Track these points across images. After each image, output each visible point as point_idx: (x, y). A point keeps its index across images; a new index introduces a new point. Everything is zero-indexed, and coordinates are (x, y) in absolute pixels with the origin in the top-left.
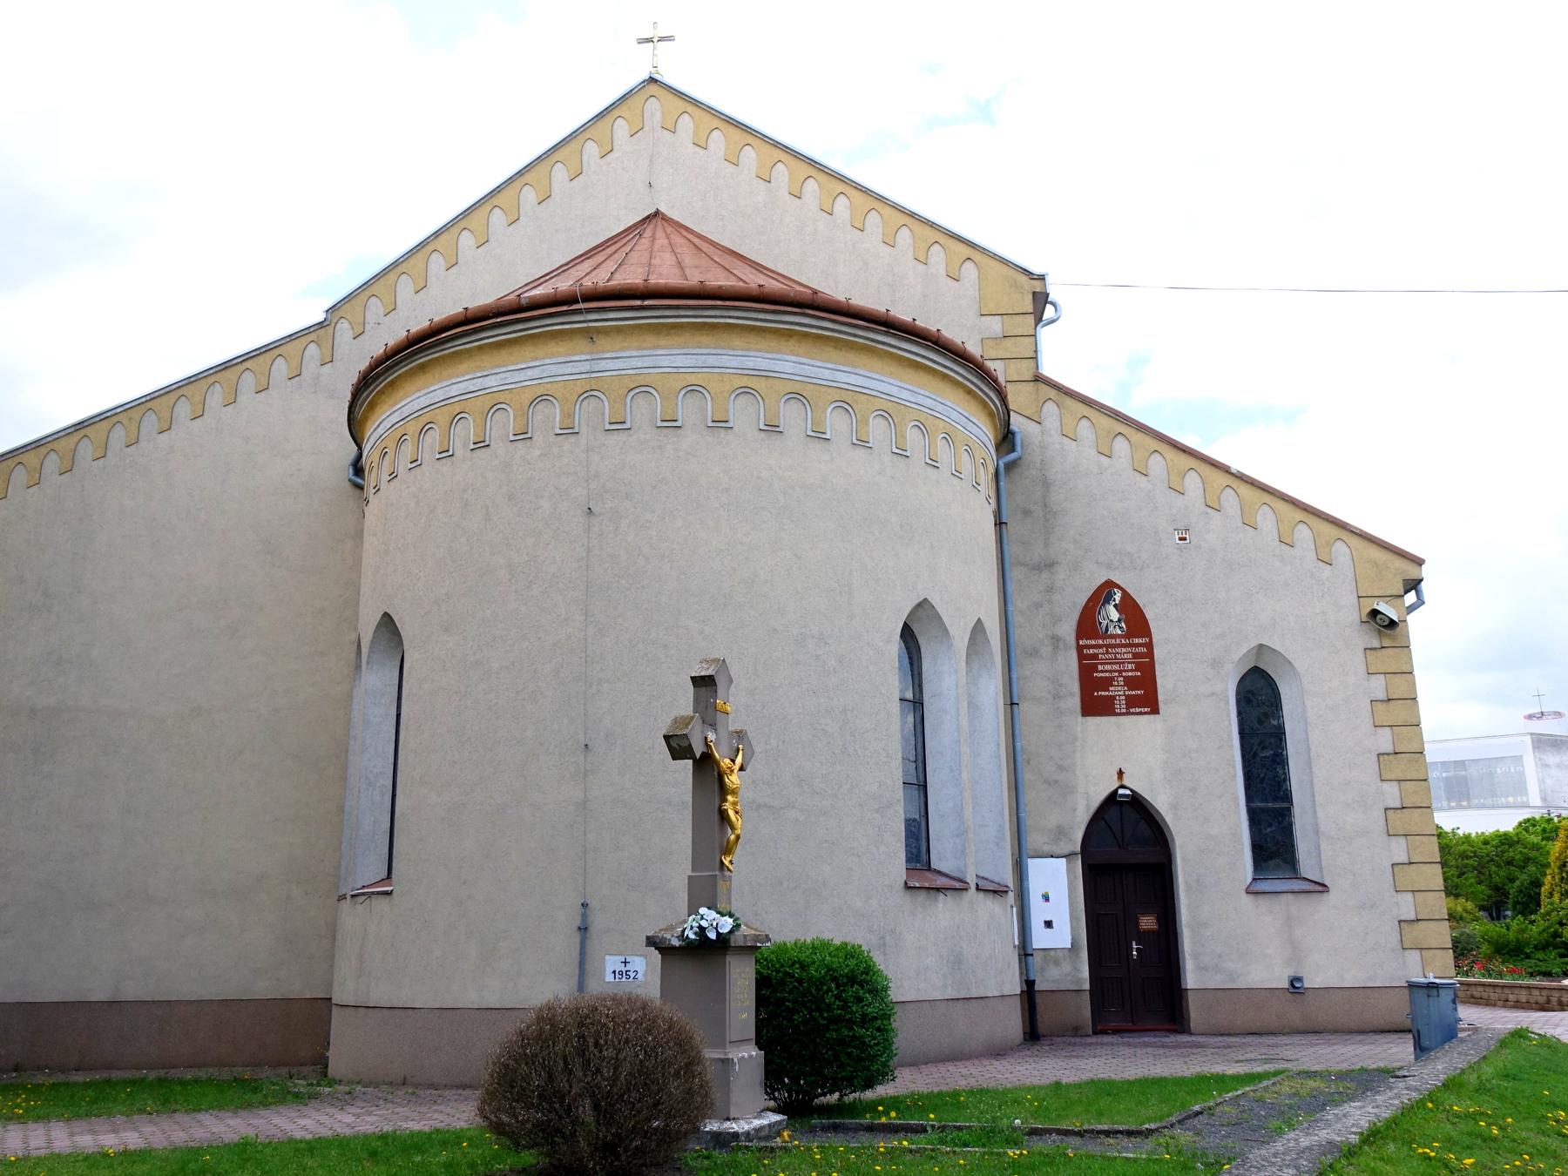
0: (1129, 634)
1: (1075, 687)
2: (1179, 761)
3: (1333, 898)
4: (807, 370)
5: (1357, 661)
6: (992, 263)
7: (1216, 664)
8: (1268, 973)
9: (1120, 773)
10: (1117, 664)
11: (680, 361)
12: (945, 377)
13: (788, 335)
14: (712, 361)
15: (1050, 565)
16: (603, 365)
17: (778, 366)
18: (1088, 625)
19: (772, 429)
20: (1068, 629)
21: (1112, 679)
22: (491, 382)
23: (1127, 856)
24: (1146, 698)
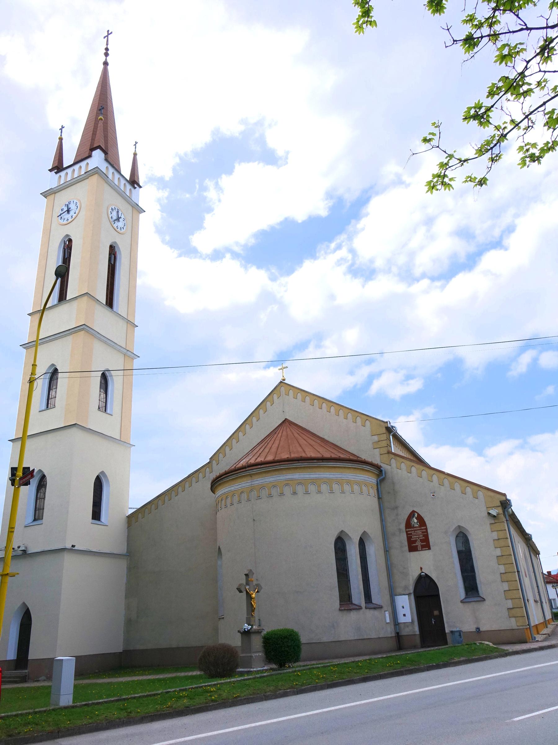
0: (420, 526)
1: (406, 543)
2: (438, 562)
3: (487, 602)
4: (302, 476)
5: (488, 527)
6: (374, 420)
7: (446, 533)
8: (468, 627)
9: (421, 568)
10: (418, 535)
11: (271, 479)
12: (345, 467)
13: (296, 468)
14: (278, 478)
15: (396, 508)
16: (254, 483)
17: (295, 477)
18: (408, 524)
19: (295, 493)
20: (403, 526)
21: (416, 540)
22: (232, 488)
23: (426, 593)
24: (426, 545)
